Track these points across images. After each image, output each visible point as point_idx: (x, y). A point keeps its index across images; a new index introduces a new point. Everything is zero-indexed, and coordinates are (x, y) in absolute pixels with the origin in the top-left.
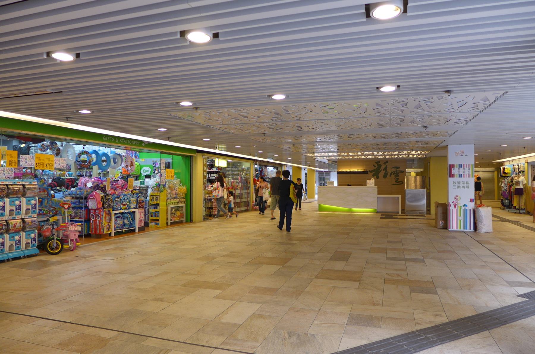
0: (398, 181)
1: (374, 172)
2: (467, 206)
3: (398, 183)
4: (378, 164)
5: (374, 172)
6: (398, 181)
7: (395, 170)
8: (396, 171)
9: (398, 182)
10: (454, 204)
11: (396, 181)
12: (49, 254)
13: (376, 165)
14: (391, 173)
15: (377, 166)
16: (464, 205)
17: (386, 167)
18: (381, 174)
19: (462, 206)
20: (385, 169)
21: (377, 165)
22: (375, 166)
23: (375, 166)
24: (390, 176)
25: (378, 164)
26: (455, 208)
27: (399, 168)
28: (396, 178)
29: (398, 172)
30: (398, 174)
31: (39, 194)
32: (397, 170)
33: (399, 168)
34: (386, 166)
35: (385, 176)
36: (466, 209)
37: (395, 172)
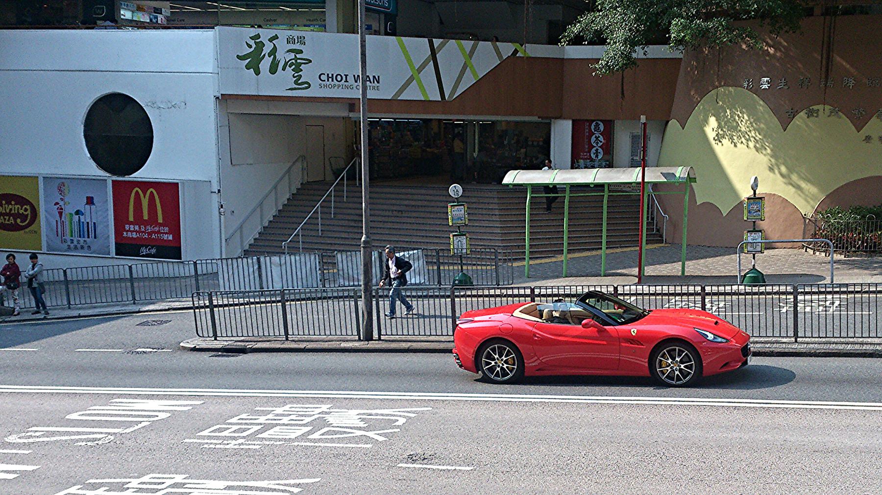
0: (299, 82)
1: (249, 60)
2: (83, 214)
3: (300, 87)
4: (257, 41)
5: (249, 60)
6: (299, 82)
7: (292, 56)
8: (296, 59)
9: (299, 84)
10: (58, 209)
11: (296, 82)
12: (38, 217)
13: (252, 43)
14: (286, 63)
15: (254, 46)
16: (78, 212)
17: (275, 49)
18: (265, 64)
19: (73, 213)
20: (273, 52)
21: (255, 42)
22: (250, 46)
23: (250, 46)
24: (284, 69)
25: (257, 41)
26: (61, 218)
27: (301, 52)
28: (296, 75)
29: (298, 61)
30: (300, 66)
31: (729, 29)
32: (298, 56)
33: (301, 52)
34: (274, 44)
35: (273, 70)
36: (82, 220)
37: (293, 61)
